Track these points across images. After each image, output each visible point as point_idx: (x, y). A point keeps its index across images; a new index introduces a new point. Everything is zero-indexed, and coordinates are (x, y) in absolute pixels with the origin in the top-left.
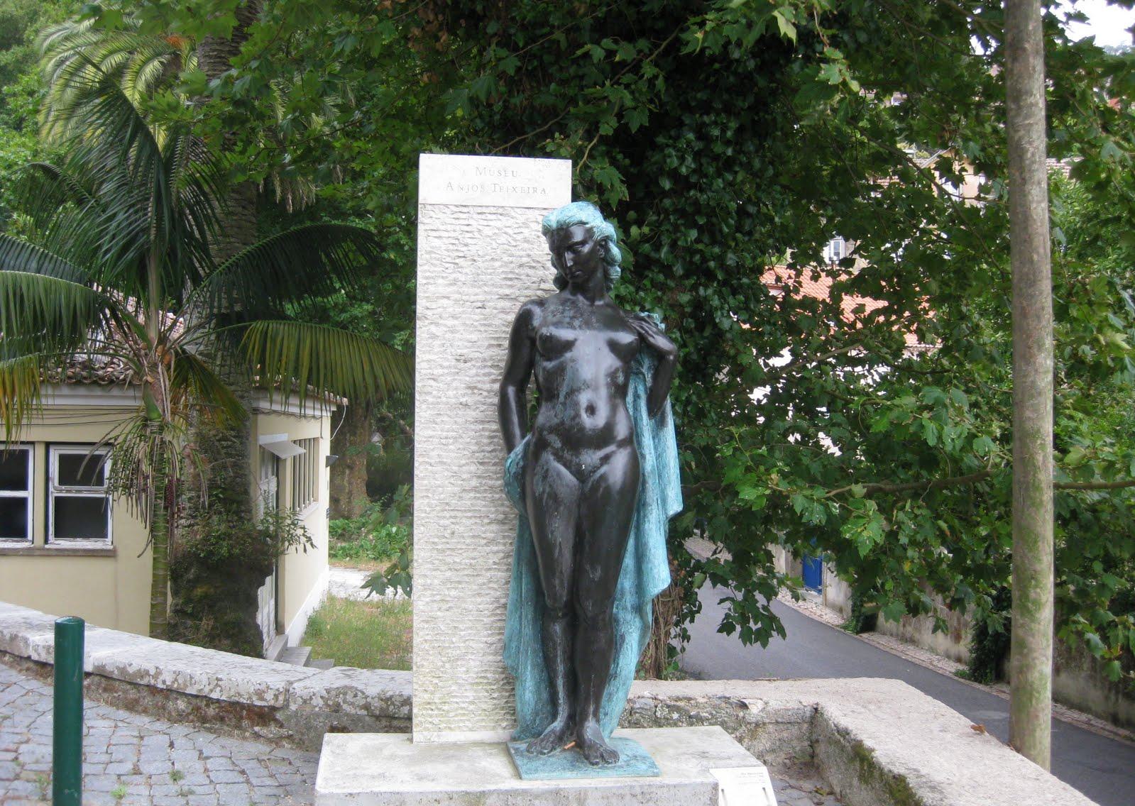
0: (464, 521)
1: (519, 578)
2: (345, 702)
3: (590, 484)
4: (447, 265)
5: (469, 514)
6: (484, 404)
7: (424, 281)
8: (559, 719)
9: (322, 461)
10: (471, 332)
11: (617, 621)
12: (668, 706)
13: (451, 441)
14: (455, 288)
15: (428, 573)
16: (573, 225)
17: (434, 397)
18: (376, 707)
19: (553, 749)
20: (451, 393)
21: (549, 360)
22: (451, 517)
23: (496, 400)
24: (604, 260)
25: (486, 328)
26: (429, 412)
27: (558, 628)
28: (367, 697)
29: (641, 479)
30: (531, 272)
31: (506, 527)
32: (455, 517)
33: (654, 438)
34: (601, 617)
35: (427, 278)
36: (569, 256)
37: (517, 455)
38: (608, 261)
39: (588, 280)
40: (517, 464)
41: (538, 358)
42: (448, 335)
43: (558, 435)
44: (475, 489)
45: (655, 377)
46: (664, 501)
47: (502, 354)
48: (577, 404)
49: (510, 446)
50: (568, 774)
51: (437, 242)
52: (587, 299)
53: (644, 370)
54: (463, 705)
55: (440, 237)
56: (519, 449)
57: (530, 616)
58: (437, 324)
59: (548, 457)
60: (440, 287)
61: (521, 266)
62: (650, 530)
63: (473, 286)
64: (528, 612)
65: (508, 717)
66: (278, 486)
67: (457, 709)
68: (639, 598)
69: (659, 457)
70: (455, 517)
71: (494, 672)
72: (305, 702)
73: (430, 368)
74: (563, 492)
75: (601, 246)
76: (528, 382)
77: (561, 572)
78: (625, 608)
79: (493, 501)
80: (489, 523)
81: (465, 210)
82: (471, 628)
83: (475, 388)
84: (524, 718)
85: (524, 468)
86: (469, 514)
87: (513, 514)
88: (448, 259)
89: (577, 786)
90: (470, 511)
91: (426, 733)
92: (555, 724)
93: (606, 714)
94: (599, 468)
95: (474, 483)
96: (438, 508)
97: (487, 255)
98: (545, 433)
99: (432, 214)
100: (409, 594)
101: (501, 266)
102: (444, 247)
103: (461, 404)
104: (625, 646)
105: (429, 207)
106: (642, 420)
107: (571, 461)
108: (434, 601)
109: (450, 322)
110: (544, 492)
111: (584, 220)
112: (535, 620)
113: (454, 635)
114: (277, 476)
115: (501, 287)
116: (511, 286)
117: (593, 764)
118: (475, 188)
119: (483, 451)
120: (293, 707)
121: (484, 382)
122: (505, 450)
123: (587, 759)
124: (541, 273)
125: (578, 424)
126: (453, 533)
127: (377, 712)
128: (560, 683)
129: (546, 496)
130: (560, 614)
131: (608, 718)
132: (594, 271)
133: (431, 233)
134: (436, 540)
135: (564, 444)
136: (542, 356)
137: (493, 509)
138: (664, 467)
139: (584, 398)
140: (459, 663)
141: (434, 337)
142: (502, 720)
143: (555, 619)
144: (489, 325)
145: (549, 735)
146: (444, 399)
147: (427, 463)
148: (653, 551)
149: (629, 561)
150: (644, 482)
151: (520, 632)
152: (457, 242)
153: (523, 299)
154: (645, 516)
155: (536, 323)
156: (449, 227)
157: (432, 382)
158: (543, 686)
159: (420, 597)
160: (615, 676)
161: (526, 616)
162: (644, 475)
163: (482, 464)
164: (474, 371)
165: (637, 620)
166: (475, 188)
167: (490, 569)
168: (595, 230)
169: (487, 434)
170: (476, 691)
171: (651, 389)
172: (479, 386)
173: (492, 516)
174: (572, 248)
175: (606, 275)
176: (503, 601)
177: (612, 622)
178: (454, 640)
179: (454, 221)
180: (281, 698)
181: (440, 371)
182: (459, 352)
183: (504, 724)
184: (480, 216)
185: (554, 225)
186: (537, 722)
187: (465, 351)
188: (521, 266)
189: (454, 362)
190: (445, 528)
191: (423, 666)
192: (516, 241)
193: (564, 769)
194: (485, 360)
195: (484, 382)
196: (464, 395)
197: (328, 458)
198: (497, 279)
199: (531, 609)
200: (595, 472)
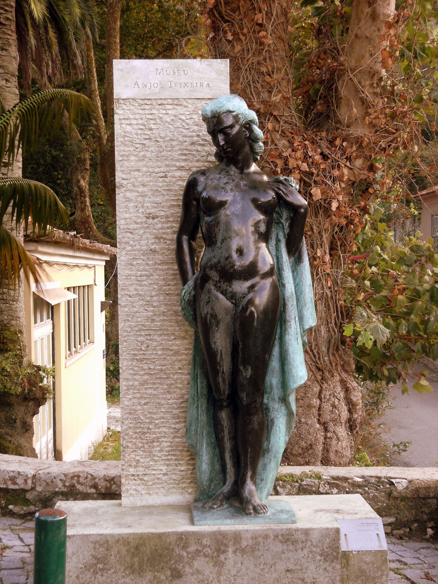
0: (156, 337)
1: (195, 379)
2: (78, 483)
3: (241, 307)
4: (138, 146)
5: (160, 332)
6: (169, 250)
7: (120, 159)
8: (227, 484)
9: (97, 306)
10: (157, 196)
11: (267, 409)
12: (329, 483)
13: (145, 278)
14: (144, 163)
15: (130, 377)
16: (223, 113)
17: (131, 246)
18: (102, 487)
19: (221, 505)
20: (143, 242)
21: (209, 216)
22: (146, 335)
23: (174, 247)
24: (249, 138)
25: (169, 193)
26: (128, 257)
27: (224, 415)
28: (95, 479)
29: (281, 302)
30: (200, 148)
31: (186, 341)
32: (150, 335)
33: (293, 272)
34: (253, 406)
35: (122, 156)
36: (221, 137)
37: (189, 287)
38: (254, 139)
39: (237, 154)
40: (190, 293)
41: (202, 214)
42: (139, 199)
43: (216, 271)
44: (164, 314)
45: (291, 226)
46: (301, 319)
47: (179, 211)
48: (229, 249)
49: (185, 281)
50: (228, 521)
51: (129, 128)
52: (237, 168)
53: (283, 221)
54: (159, 476)
55: (130, 124)
56: (191, 283)
57: (204, 407)
58: (131, 191)
59: (210, 286)
60: (133, 162)
61: (193, 144)
62: (290, 340)
63: (157, 161)
64: (203, 403)
65: (192, 485)
66: (53, 329)
67: (154, 479)
68: (284, 391)
69: (297, 286)
70: (150, 335)
71: (181, 451)
72: (48, 484)
73: (127, 224)
74: (221, 315)
75: (246, 128)
76: (197, 233)
77: (223, 372)
78: (273, 399)
79: (177, 322)
80: (175, 339)
81: (149, 102)
82: (163, 418)
83: (162, 238)
84: (202, 484)
85: (195, 296)
86: (160, 332)
87: (191, 331)
88: (138, 141)
89: (233, 529)
90: (160, 330)
91: (131, 498)
92: (224, 487)
93: (262, 480)
94: (247, 294)
95: (163, 309)
96: (136, 329)
97: (167, 136)
98: (207, 270)
99: (124, 107)
100: (337, 494)
101: (177, 145)
102: (134, 132)
103: (151, 250)
104: (274, 428)
105: (122, 101)
106: (282, 258)
107: (226, 290)
108: (135, 398)
109: (141, 189)
110: (207, 313)
111: (231, 109)
112: (208, 409)
113: (150, 423)
114: (52, 319)
115: (178, 160)
116: (185, 160)
117: (247, 514)
118: (156, 85)
119: (169, 285)
120: (39, 489)
121: (167, 234)
122: (180, 282)
123: (244, 511)
124: (207, 149)
125: (230, 263)
126: (148, 346)
127: (103, 491)
128: (228, 456)
129: (209, 316)
130: (225, 404)
131: (264, 482)
132: (243, 146)
133: (123, 122)
134: (136, 352)
135: (221, 278)
136: (204, 213)
137: (178, 328)
138: (301, 293)
139: (235, 244)
140: (155, 444)
141: (129, 200)
142: (188, 487)
143: (221, 408)
144: (170, 190)
145: (219, 495)
146: (138, 247)
147: (127, 295)
148: (292, 356)
149: (275, 364)
150: (284, 305)
151: (197, 418)
152: (144, 128)
153: (194, 169)
154: (285, 330)
155: (200, 188)
156: (137, 116)
157: (129, 234)
158: (216, 459)
159: (124, 394)
160: (268, 450)
161: (201, 407)
162: (284, 299)
163: (167, 294)
164: (160, 225)
165: (283, 408)
166: (156, 85)
167: (177, 373)
168: (240, 116)
169: (171, 272)
170: (168, 465)
171: (289, 235)
172: (164, 236)
173: (177, 334)
174: (223, 131)
175: (252, 149)
176: (186, 397)
177: (265, 410)
178: (151, 427)
179: (140, 111)
180: (30, 482)
181: (135, 226)
182: (148, 211)
183: (190, 491)
184: (160, 107)
185: (209, 114)
186: (212, 487)
187: (152, 211)
188: (193, 144)
189: (144, 219)
190: (142, 343)
191: (128, 446)
192: (188, 125)
193: (226, 518)
194: (167, 217)
195: (167, 234)
196: (153, 244)
197: (103, 304)
198: (176, 155)
199: (206, 401)
200: (244, 297)
